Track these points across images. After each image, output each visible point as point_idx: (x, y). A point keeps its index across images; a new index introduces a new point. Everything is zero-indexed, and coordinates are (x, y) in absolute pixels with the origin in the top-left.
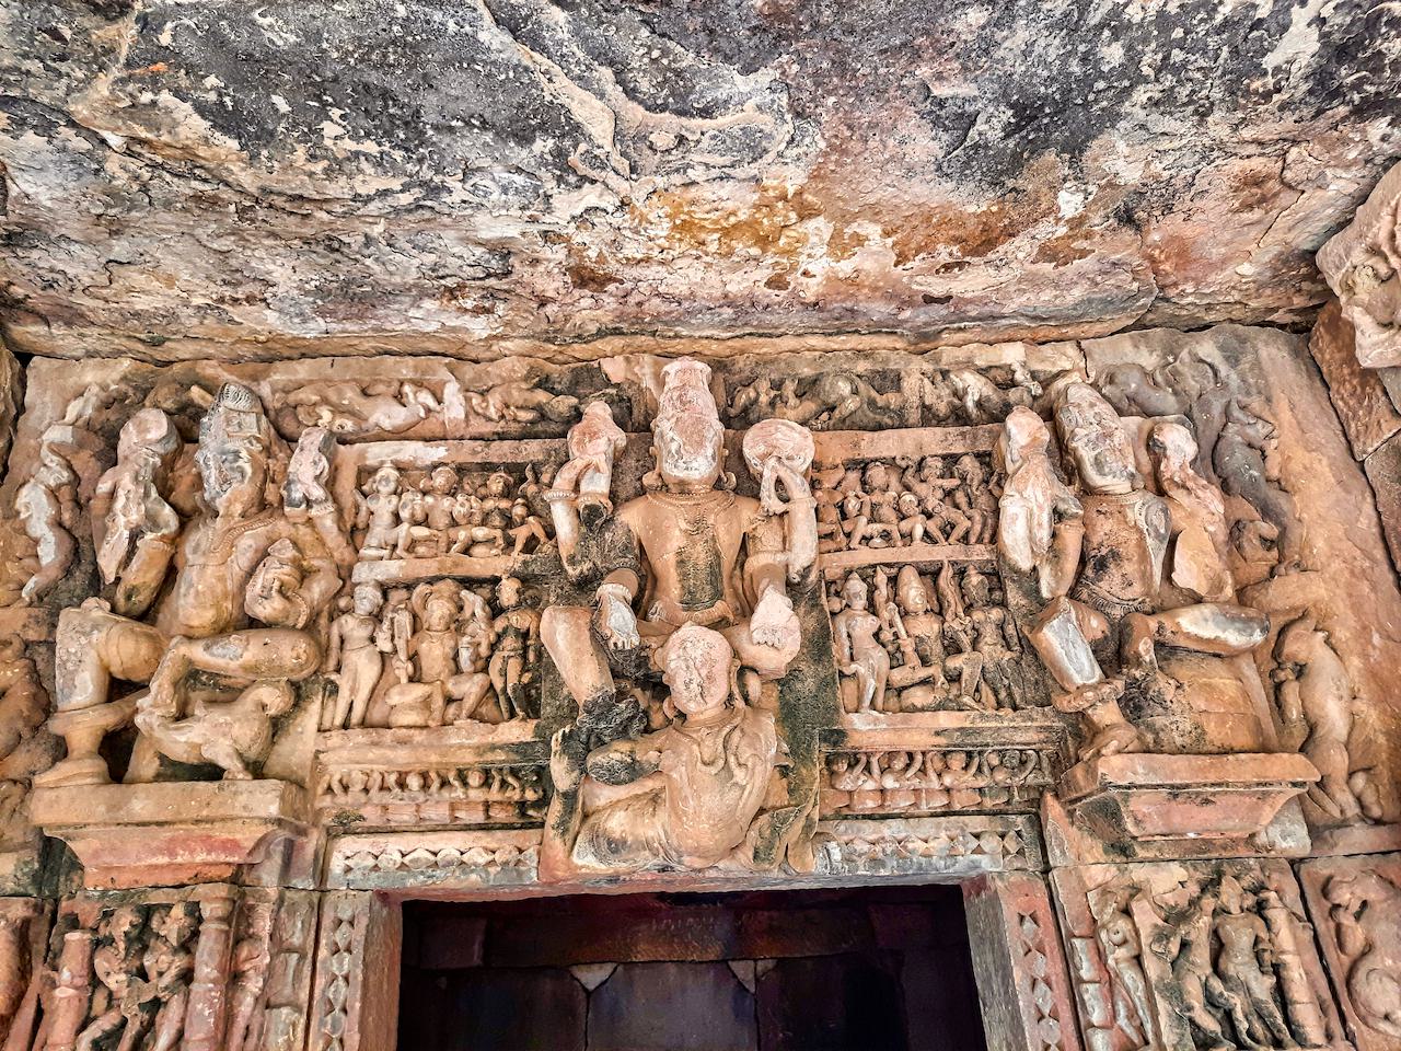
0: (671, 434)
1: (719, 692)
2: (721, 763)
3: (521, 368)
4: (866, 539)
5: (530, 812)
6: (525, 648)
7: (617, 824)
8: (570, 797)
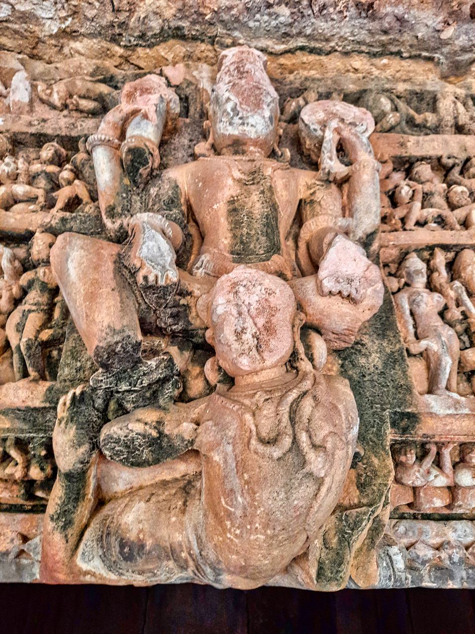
0: (227, 95)
1: (282, 344)
2: (287, 441)
3: (89, 65)
4: (420, 224)
5: (39, 494)
6: (52, 306)
7: (132, 519)
8: (76, 479)
